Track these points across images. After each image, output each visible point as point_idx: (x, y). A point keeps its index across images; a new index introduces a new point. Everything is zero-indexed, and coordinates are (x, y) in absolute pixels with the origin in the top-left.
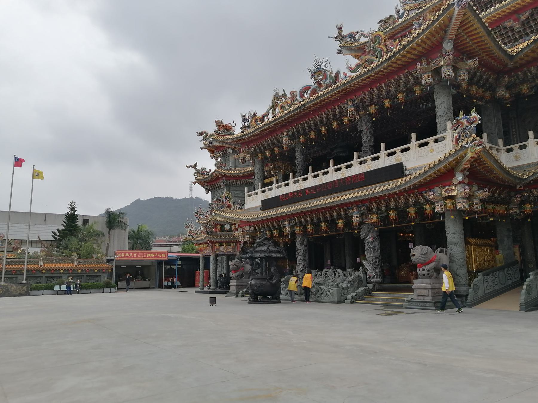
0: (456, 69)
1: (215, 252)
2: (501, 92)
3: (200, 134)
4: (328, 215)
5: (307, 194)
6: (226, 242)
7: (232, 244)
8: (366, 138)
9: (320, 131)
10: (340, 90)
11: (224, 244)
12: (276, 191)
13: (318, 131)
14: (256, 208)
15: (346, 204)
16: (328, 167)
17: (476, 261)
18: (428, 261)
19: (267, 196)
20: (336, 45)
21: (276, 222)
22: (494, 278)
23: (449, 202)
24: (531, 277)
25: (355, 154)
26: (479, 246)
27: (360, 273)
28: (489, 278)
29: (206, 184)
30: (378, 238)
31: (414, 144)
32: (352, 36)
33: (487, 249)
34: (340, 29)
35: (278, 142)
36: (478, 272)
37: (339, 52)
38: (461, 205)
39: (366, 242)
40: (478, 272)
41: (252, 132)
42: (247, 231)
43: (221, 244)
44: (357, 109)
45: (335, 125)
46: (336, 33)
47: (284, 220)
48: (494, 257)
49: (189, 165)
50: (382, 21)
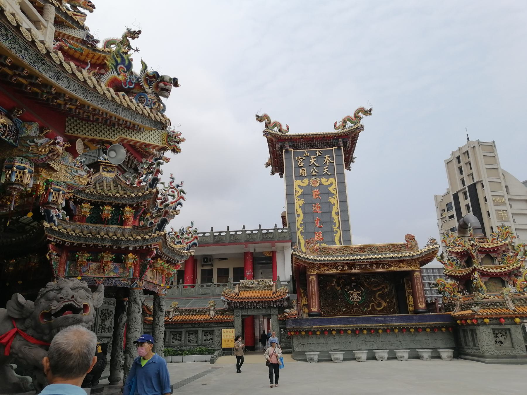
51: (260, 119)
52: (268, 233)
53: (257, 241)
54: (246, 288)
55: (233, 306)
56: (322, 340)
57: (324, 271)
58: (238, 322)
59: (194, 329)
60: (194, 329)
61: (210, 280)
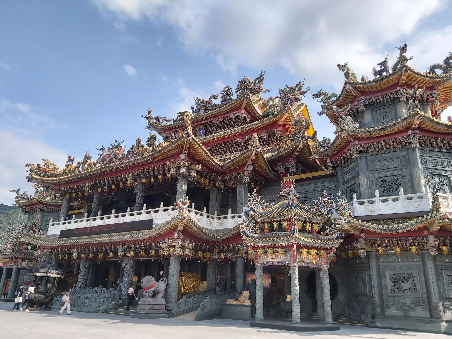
0: (188, 169)
1: (18, 266)
2: (219, 184)
3: (28, 166)
4: (103, 248)
5: (93, 230)
6: (28, 259)
7: (33, 261)
8: (139, 198)
9: (111, 187)
10: (123, 166)
11: (27, 260)
12: (73, 225)
13: (110, 187)
14: (55, 235)
15: (116, 242)
16: (111, 213)
17: (184, 288)
18: (150, 286)
19: (66, 227)
20: (145, 123)
21: (67, 248)
22: (194, 299)
23: (172, 249)
24: (207, 300)
25: (129, 208)
26: (189, 278)
27: (116, 292)
28: (191, 299)
29: (24, 207)
30: (134, 267)
31: (161, 209)
32: (158, 118)
33: (194, 280)
34: (150, 113)
35: (82, 188)
36: (183, 295)
37: (148, 128)
38: (178, 252)
39: (125, 270)
40: (183, 295)
41: (63, 179)
42: (45, 252)
43: (24, 260)
44: (134, 178)
45: (121, 185)
46: (147, 114)
47: (74, 248)
48: (199, 285)
49: (12, 190)
50: (180, 113)
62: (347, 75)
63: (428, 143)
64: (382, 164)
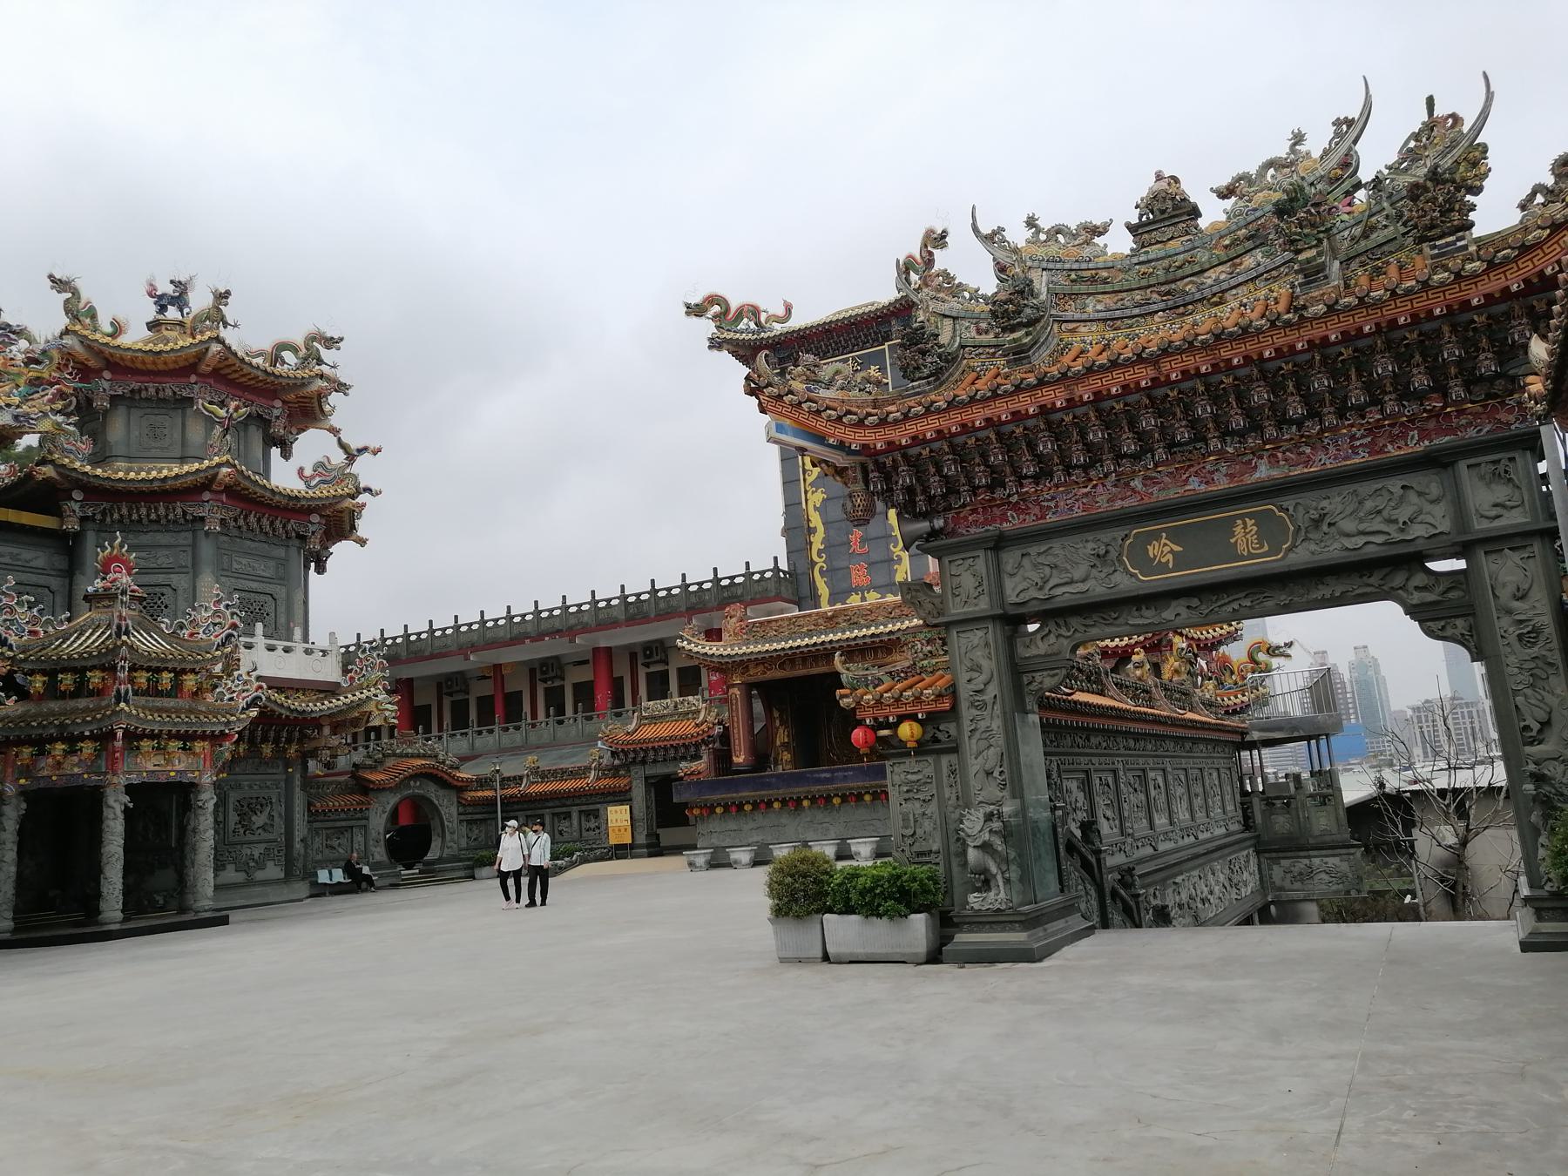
51: (696, 310)
52: (732, 584)
53: (710, 605)
54: (655, 719)
55: (629, 757)
56: (732, 825)
57: (757, 674)
58: (639, 791)
59: (564, 809)
60: (564, 809)
61: (561, 711)
62: (71, 310)
63: (241, 522)
64: (244, 561)
